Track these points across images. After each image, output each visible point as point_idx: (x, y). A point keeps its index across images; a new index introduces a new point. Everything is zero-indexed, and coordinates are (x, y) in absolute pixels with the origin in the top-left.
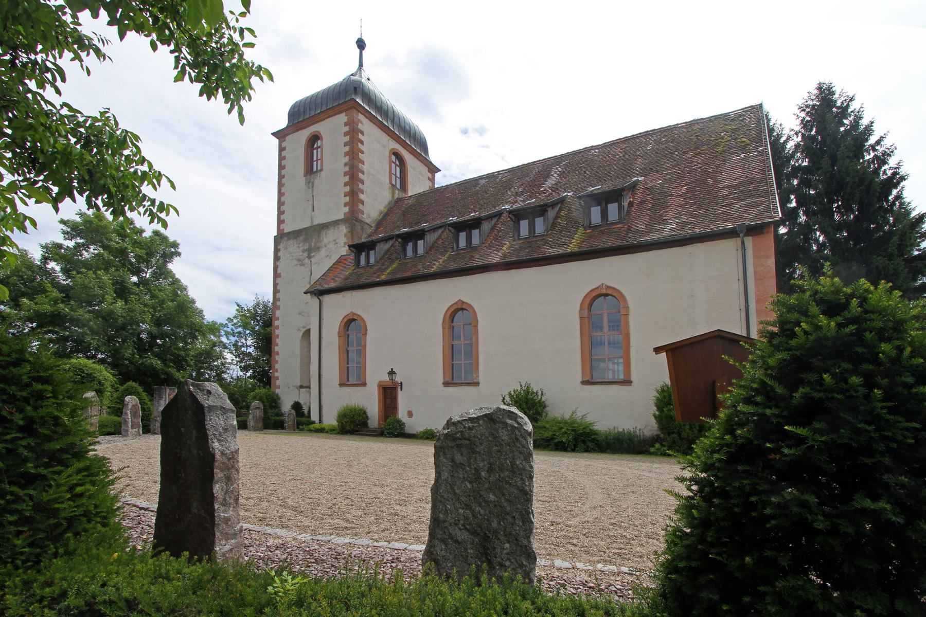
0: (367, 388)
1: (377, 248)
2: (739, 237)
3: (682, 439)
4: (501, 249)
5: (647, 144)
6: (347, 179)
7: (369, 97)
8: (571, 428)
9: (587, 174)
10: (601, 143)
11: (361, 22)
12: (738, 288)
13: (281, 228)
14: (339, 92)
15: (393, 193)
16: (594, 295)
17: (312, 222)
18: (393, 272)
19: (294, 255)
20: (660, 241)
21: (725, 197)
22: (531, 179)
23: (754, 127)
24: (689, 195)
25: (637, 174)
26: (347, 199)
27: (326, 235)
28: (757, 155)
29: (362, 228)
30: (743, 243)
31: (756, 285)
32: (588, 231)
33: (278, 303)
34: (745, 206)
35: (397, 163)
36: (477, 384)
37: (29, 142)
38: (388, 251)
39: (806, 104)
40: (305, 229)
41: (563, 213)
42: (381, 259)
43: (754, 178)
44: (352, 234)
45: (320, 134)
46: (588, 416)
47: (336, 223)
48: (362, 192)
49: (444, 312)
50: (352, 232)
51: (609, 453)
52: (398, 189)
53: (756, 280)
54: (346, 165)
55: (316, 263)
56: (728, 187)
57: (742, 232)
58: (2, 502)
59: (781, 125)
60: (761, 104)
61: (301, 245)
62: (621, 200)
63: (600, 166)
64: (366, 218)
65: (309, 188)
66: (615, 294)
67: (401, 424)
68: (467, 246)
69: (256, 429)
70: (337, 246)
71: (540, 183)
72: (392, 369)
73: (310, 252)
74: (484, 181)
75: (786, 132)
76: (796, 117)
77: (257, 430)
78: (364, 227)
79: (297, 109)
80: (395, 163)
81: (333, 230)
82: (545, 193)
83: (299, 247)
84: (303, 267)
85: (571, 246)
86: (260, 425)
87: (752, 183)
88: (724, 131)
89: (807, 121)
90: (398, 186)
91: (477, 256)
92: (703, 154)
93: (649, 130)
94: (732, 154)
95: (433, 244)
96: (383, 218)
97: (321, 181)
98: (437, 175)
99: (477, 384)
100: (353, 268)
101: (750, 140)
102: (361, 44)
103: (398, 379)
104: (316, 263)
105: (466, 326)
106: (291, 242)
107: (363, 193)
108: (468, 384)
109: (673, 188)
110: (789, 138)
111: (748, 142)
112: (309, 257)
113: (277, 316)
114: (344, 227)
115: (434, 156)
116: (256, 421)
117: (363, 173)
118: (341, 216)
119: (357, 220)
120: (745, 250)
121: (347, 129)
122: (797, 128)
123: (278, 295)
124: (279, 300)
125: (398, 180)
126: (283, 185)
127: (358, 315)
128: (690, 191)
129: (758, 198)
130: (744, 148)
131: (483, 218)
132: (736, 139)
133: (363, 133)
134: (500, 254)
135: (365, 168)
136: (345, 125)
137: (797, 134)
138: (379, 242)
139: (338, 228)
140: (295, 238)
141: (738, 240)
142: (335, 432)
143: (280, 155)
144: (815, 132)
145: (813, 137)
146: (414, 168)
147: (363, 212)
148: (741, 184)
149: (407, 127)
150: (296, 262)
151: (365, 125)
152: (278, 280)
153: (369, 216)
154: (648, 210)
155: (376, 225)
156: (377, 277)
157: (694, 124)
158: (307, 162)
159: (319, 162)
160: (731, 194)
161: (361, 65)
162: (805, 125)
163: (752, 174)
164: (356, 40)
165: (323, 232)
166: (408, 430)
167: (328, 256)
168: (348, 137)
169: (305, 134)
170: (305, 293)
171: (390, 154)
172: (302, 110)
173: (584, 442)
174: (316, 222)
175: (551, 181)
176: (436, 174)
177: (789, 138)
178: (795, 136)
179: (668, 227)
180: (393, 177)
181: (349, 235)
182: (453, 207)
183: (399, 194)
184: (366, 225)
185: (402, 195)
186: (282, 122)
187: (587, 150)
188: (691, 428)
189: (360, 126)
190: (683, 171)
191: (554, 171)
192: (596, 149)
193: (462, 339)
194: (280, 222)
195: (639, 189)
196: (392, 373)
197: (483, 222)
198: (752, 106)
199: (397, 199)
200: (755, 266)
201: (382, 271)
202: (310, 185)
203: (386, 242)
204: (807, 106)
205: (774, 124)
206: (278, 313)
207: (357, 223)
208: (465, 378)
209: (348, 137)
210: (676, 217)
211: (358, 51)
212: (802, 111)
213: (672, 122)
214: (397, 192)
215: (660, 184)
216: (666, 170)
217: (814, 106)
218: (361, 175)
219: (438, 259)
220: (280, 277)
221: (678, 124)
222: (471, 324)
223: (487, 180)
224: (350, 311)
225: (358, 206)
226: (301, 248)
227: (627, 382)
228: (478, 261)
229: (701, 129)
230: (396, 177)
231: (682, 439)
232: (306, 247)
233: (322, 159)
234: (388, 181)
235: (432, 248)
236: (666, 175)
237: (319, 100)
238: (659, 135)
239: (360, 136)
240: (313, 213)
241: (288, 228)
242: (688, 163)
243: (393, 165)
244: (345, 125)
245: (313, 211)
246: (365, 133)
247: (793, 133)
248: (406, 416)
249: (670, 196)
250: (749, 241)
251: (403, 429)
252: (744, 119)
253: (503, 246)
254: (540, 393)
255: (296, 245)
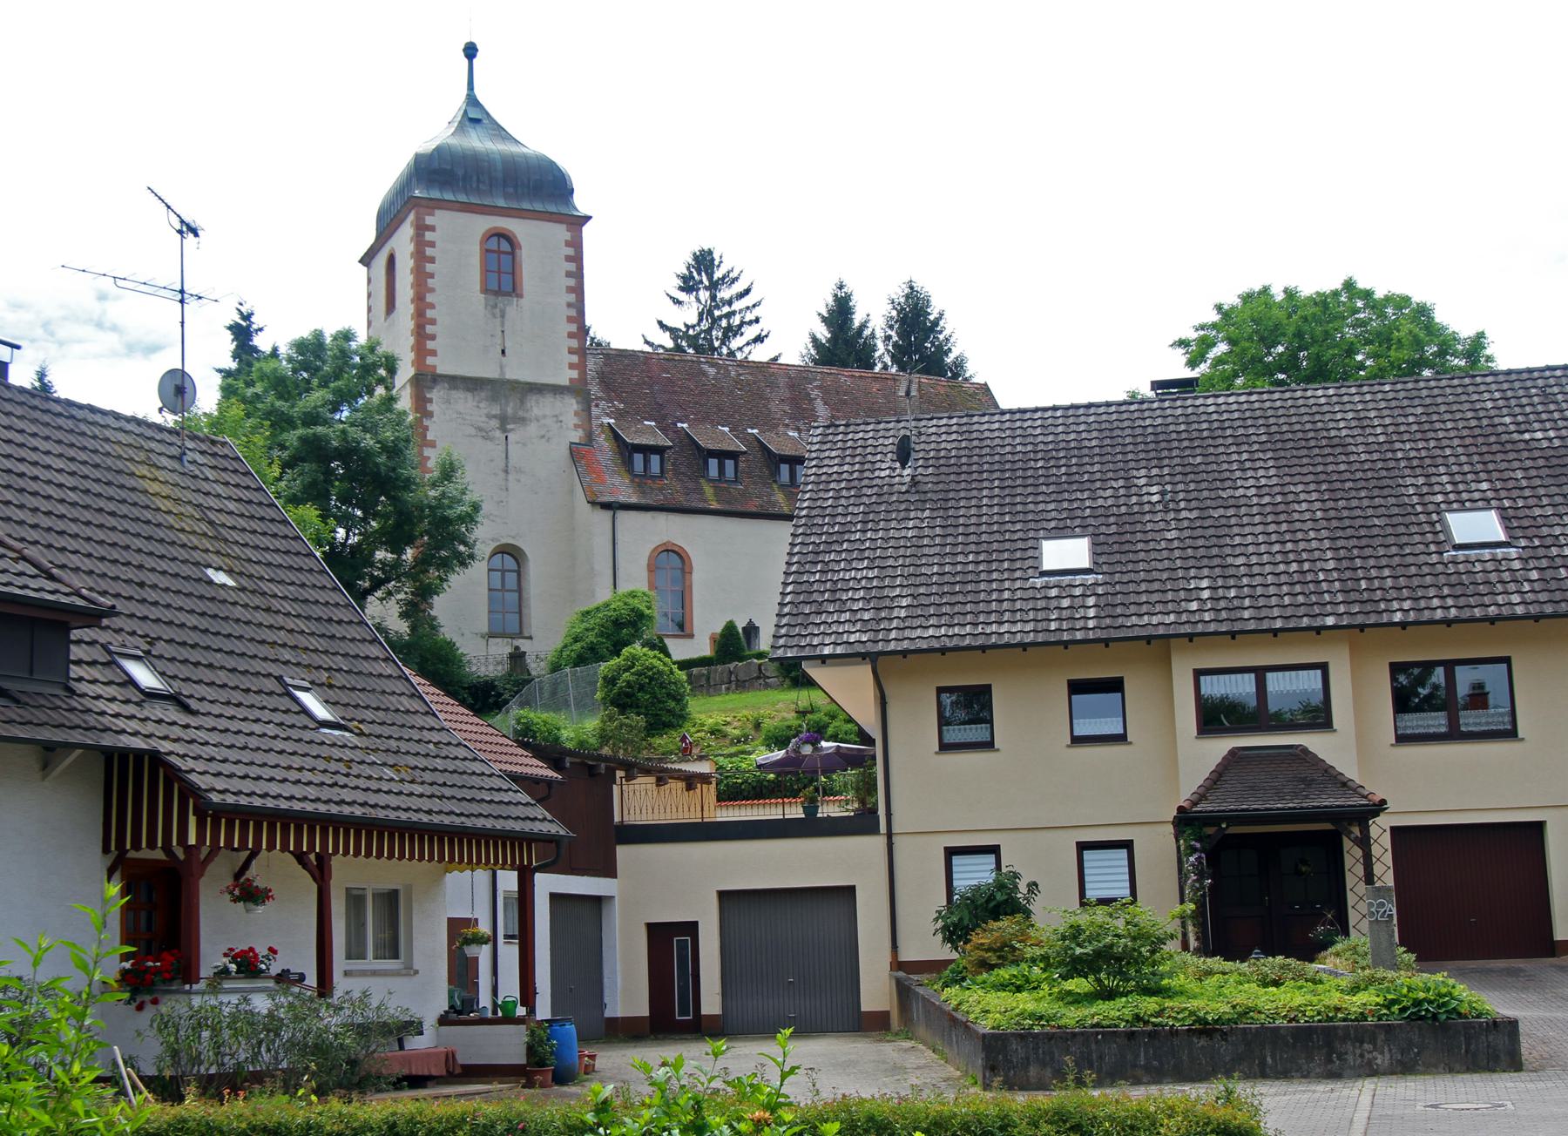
37: (601, 747)
47: (556, 390)
61: (482, 405)
65: (494, 316)
84: (488, 442)
150: (473, 432)
167: (543, 437)
174: (511, 375)
232: (496, 410)
240: (504, 359)
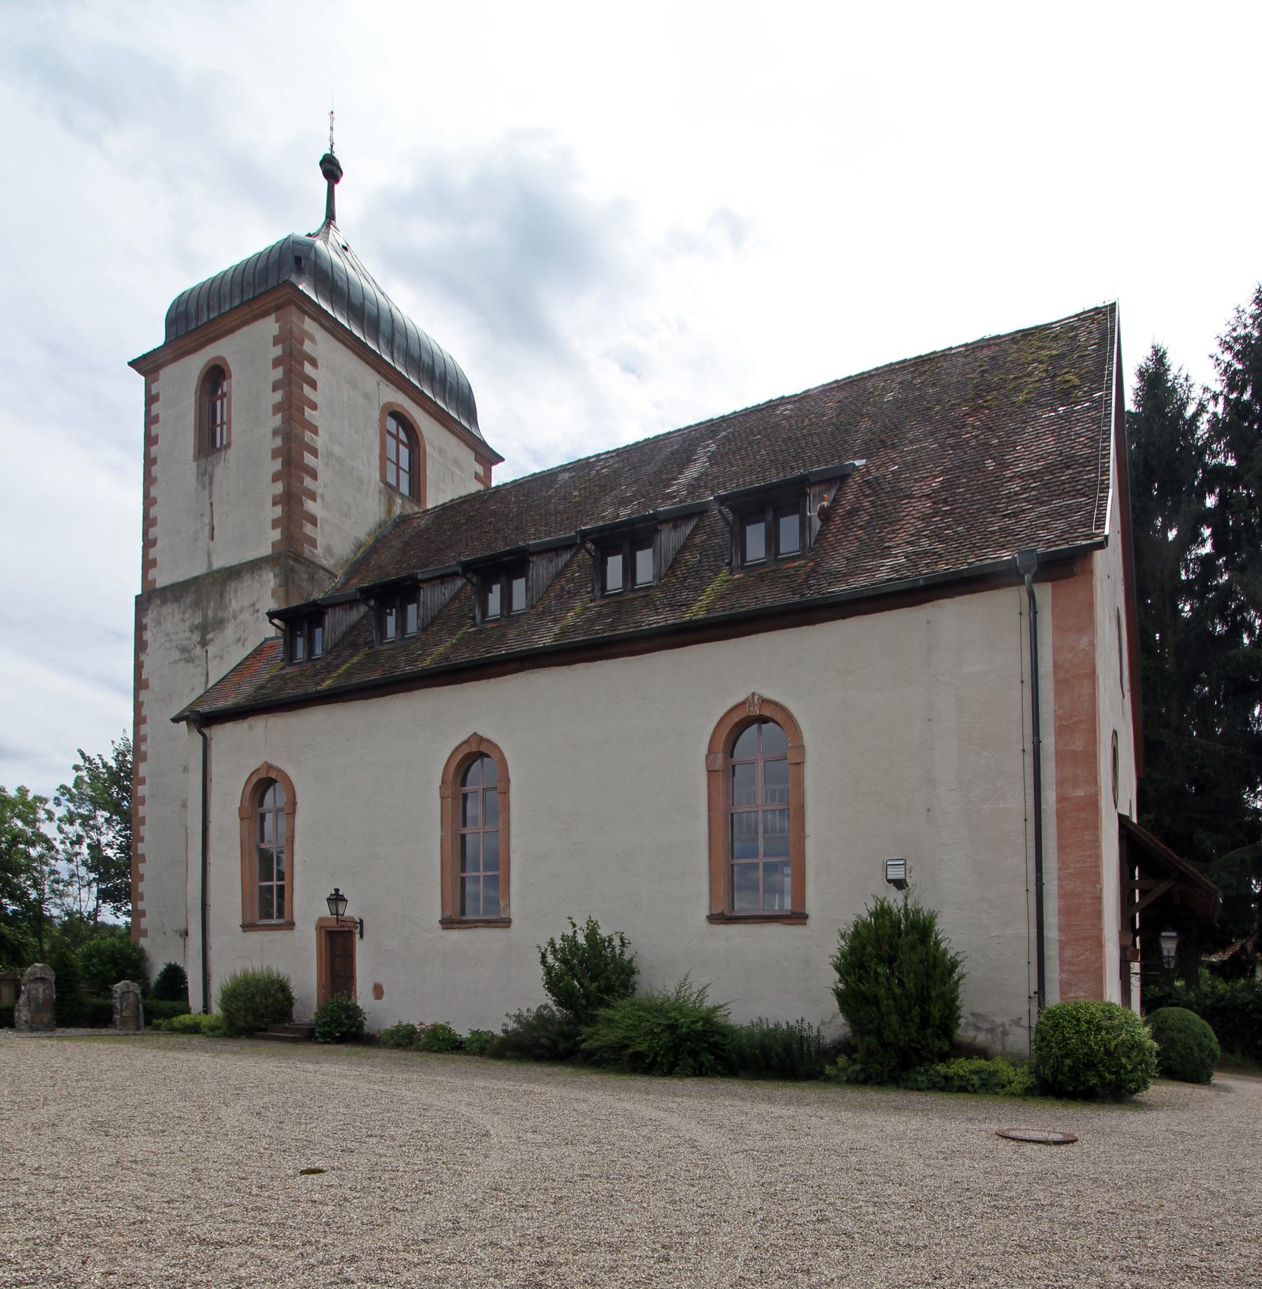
0: (296, 933)
1: (328, 620)
2: (1022, 583)
3: (885, 1046)
4: (563, 618)
5: (885, 390)
6: (277, 465)
7: (329, 281)
8: (665, 1022)
9: (762, 455)
10: (799, 390)
11: (332, 119)
12: (1019, 699)
13: (150, 578)
14: (266, 268)
15: (390, 504)
16: (737, 720)
17: (210, 564)
18: (349, 674)
19: (174, 637)
20: (866, 593)
21: (1013, 497)
22: (656, 469)
23: (1094, 350)
24: (944, 495)
25: (855, 453)
26: (278, 511)
27: (236, 592)
28: (1089, 408)
29: (312, 579)
30: (1032, 597)
31: (1058, 695)
32: (736, 576)
33: (143, 747)
34: (1047, 514)
35: (402, 436)
36: (506, 923)
38: (353, 627)
39: (1235, 334)
40: (195, 580)
41: (697, 540)
42: (336, 645)
43: (1074, 455)
44: (287, 592)
45: (226, 362)
46: (708, 991)
47: (255, 566)
48: (313, 496)
49: (444, 762)
50: (287, 581)
51: (743, 1078)
52: (402, 496)
53: (1058, 682)
54: (275, 433)
55: (216, 657)
56: (1021, 476)
57: (1028, 571)
58: (1259, 1042)
59: (1187, 380)
60: (1115, 304)
61: (187, 616)
62: (805, 506)
63: (790, 439)
64: (319, 554)
65: (204, 487)
66: (778, 718)
67: (354, 1013)
68: (502, 614)
69: (34, 1027)
70: (258, 619)
71: (670, 477)
72: (337, 890)
73: (206, 630)
74: (566, 476)
75: (1197, 393)
76: (1212, 362)
77: (37, 1030)
78: (317, 577)
79: (182, 308)
80: (396, 437)
81: (250, 582)
82: (675, 497)
83: (183, 620)
84: (190, 665)
85: (695, 608)
86: (47, 1017)
87: (1069, 467)
88: (1034, 361)
89: (1235, 372)
90: (405, 489)
91: (512, 633)
92: (987, 408)
93: (894, 361)
94: (1040, 406)
95: (440, 611)
96: (363, 559)
97: (228, 468)
98: (495, 469)
99: (506, 923)
100: (282, 664)
101: (1080, 377)
102: (331, 169)
103: (350, 911)
104: (216, 657)
105: (489, 794)
106: (168, 609)
107: (315, 500)
108: (489, 923)
109: (916, 481)
110: (1202, 408)
111: (1077, 382)
112: (204, 643)
113: (141, 775)
114: (271, 575)
115: (489, 428)
116: (37, 1008)
117: (314, 453)
118: (265, 550)
119: (298, 558)
120: (1035, 613)
121: (278, 351)
122: (1218, 387)
123: (144, 729)
124: (144, 739)
125: (404, 478)
126: (154, 480)
127: (279, 770)
128: (947, 486)
129: (1074, 497)
130: (1066, 395)
131: (533, 550)
132: (1055, 375)
133: (314, 363)
134: (556, 630)
135: (320, 442)
136: (275, 344)
137: (1215, 397)
138: (333, 606)
139: (260, 576)
140: (177, 599)
141: (1022, 591)
142: (218, 1032)
143: (147, 412)
144: (1251, 395)
145: (1248, 405)
146: (441, 451)
147: (313, 543)
148: (1048, 469)
149: (425, 357)
150: (176, 655)
151: (321, 345)
152: (144, 695)
153: (329, 551)
154: (861, 528)
155: (346, 574)
156: (318, 684)
157: (982, 347)
158: (200, 429)
159: (225, 427)
160: (1024, 490)
161: (330, 216)
162: (1233, 381)
163: (1072, 448)
164: (321, 158)
165: (232, 586)
166: (370, 1026)
167: (239, 640)
168: (280, 369)
169: (195, 364)
170: (176, 720)
171: (382, 413)
172: (192, 310)
173: (695, 1054)
174: (217, 565)
175: (691, 472)
176: (494, 468)
177: (1202, 408)
178: (1212, 403)
179: (889, 562)
180: (391, 468)
181: (281, 592)
182: (497, 531)
183: (403, 507)
184: (321, 572)
185: (412, 509)
186: (157, 338)
187: (771, 406)
188: (903, 1021)
189: (308, 347)
190: (941, 446)
191: (700, 451)
192: (789, 403)
193: (761, 855)
194: (148, 564)
195: (853, 484)
196: (337, 899)
197: (534, 559)
198: (1097, 308)
199: (399, 516)
200: (1057, 650)
201: (329, 669)
202: (206, 478)
203: (351, 608)
204: (1236, 339)
205: (1175, 378)
206: (143, 769)
207: (297, 566)
208: (486, 912)
209: (280, 369)
210: (908, 543)
211: (325, 183)
212: (1227, 349)
213: (940, 346)
214: (399, 501)
215: (892, 472)
216: (912, 443)
217: (1247, 337)
218: (308, 458)
219: (442, 642)
220: (147, 687)
221: (951, 349)
222: (495, 788)
223: (574, 474)
224: (264, 759)
225: (301, 526)
226: (188, 623)
227: (798, 917)
228: (514, 643)
229: (993, 358)
230: (398, 468)
231: (885, 1046)
232: (198, 620)
233: (229, 423)
234: (376, 475)
235: (435, 619)
236: (910, 452)
237: (227, 288)
238: (912, 372)
239: (308, 368)
241: (163, 579)
242: (956, 427)
243: (391, 442)
244: (275, 344)
245: (212, 538)
246: (320, 362)
247: (1208, 395)
248: (371, 995)
249: (907, 497)
250: (1044, 593)
251: (361, 1026)
252: (1077, 335)
253: (569, 611)
254: (617, 942)
255: (178, 616)
